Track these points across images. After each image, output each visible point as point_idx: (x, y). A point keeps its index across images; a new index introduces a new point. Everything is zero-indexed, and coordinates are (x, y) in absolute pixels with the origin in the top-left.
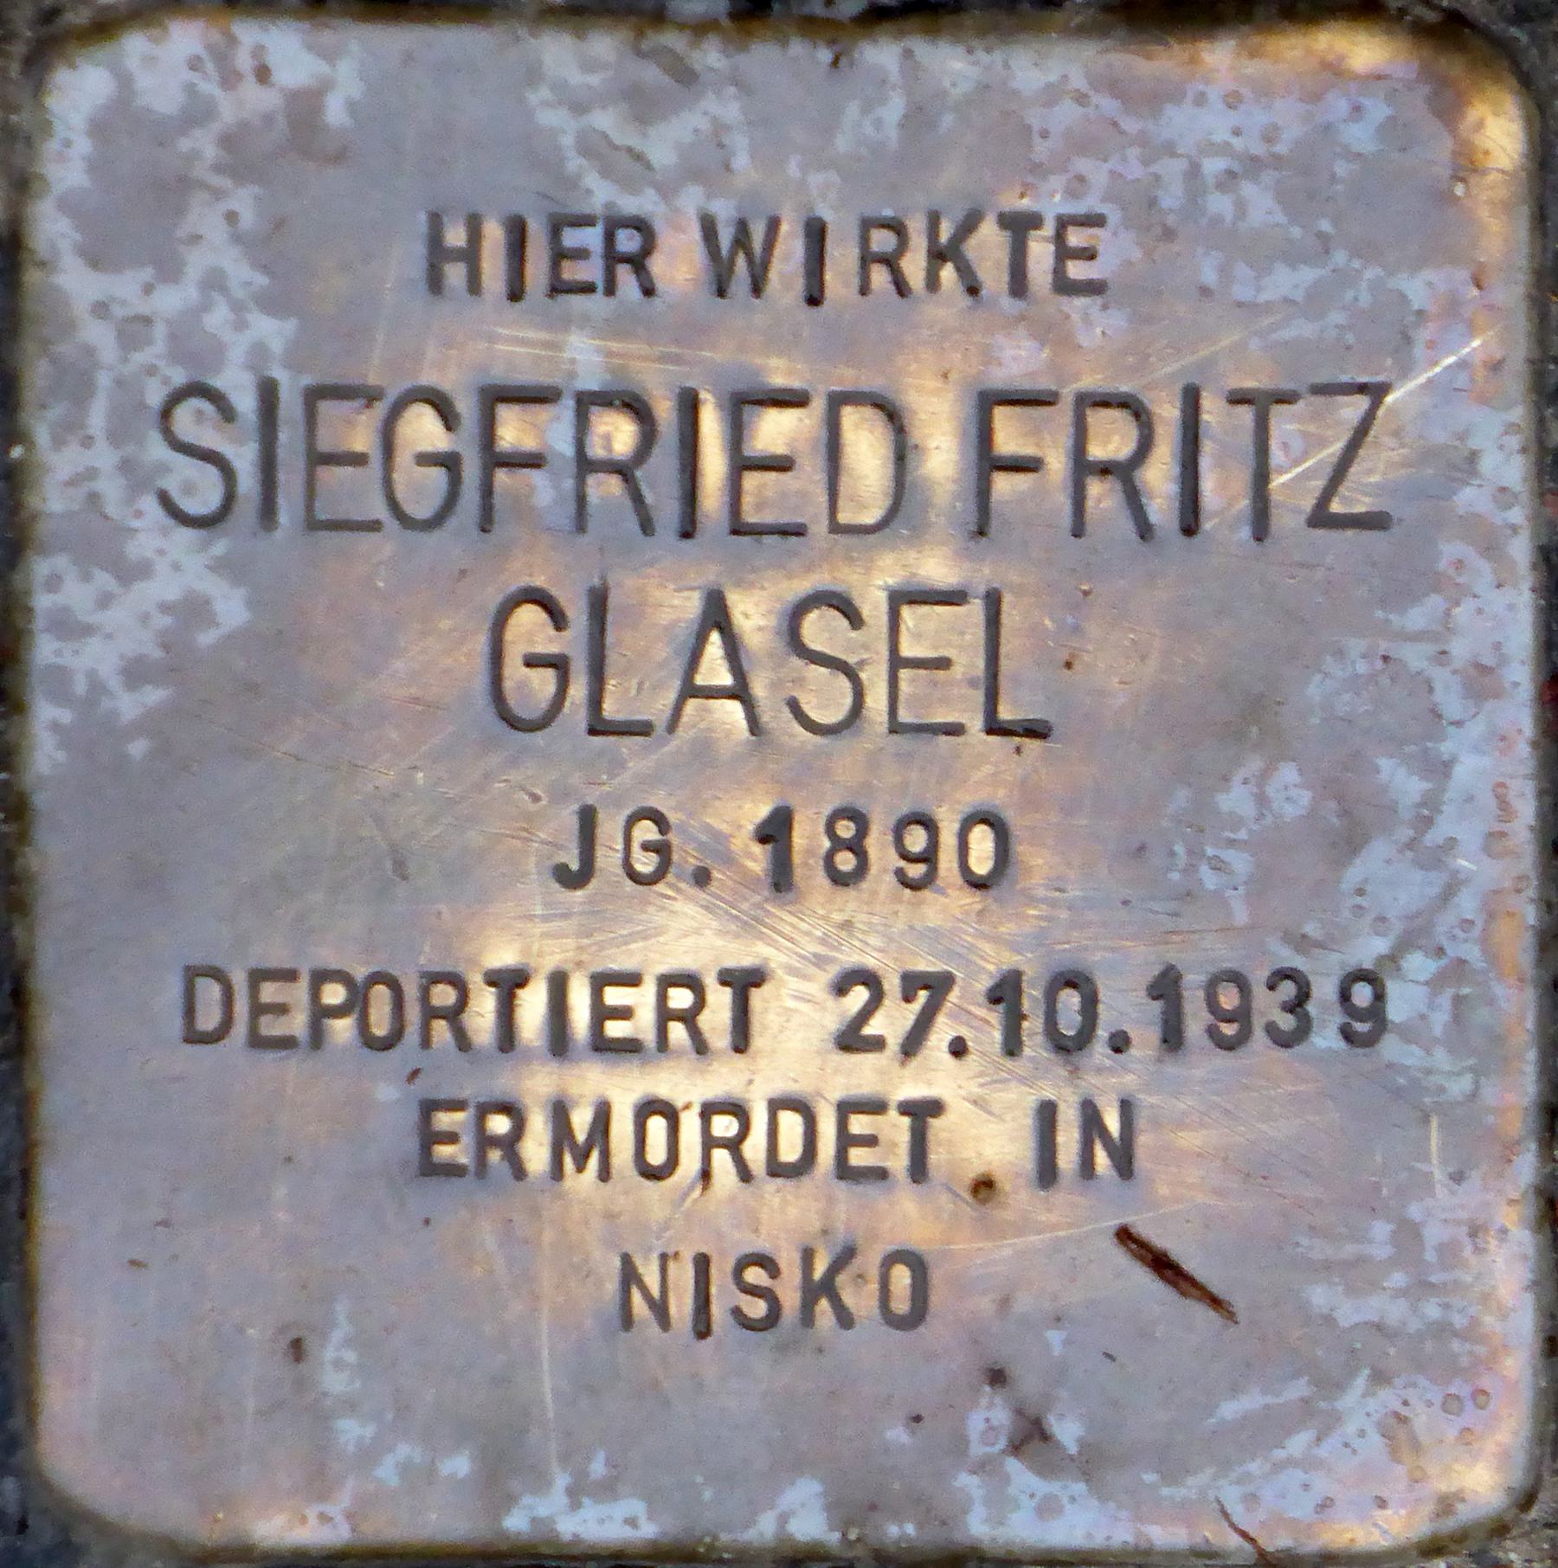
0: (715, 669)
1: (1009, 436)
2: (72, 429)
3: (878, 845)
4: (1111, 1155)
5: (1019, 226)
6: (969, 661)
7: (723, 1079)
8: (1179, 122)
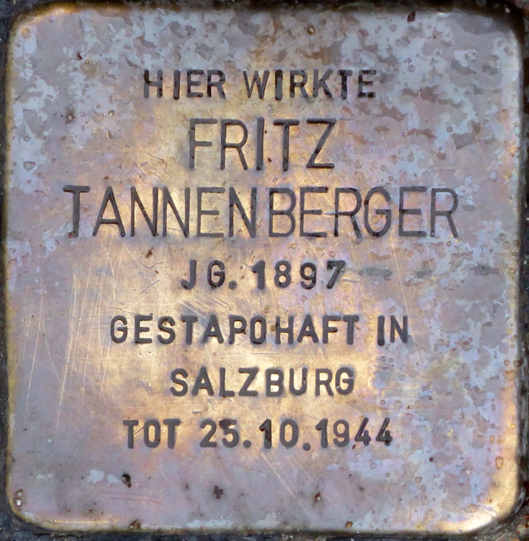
3: (295, 274)
5: (344, 75)
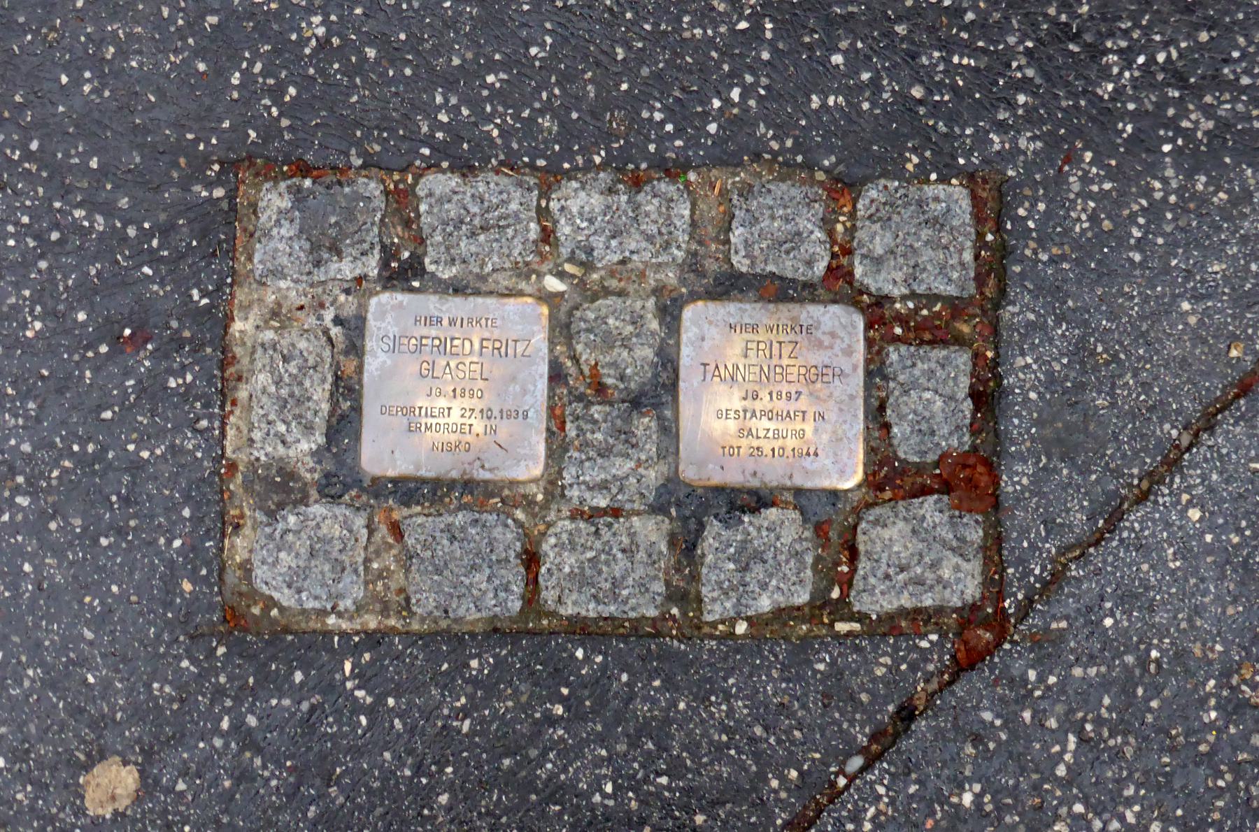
0: (447, 371)
1: (485, 343)
2: (371, 340)
4: (343, 669)
5: (487, 319)
6: (479, 371)
7: (447, 420)
8: (507, 307)
